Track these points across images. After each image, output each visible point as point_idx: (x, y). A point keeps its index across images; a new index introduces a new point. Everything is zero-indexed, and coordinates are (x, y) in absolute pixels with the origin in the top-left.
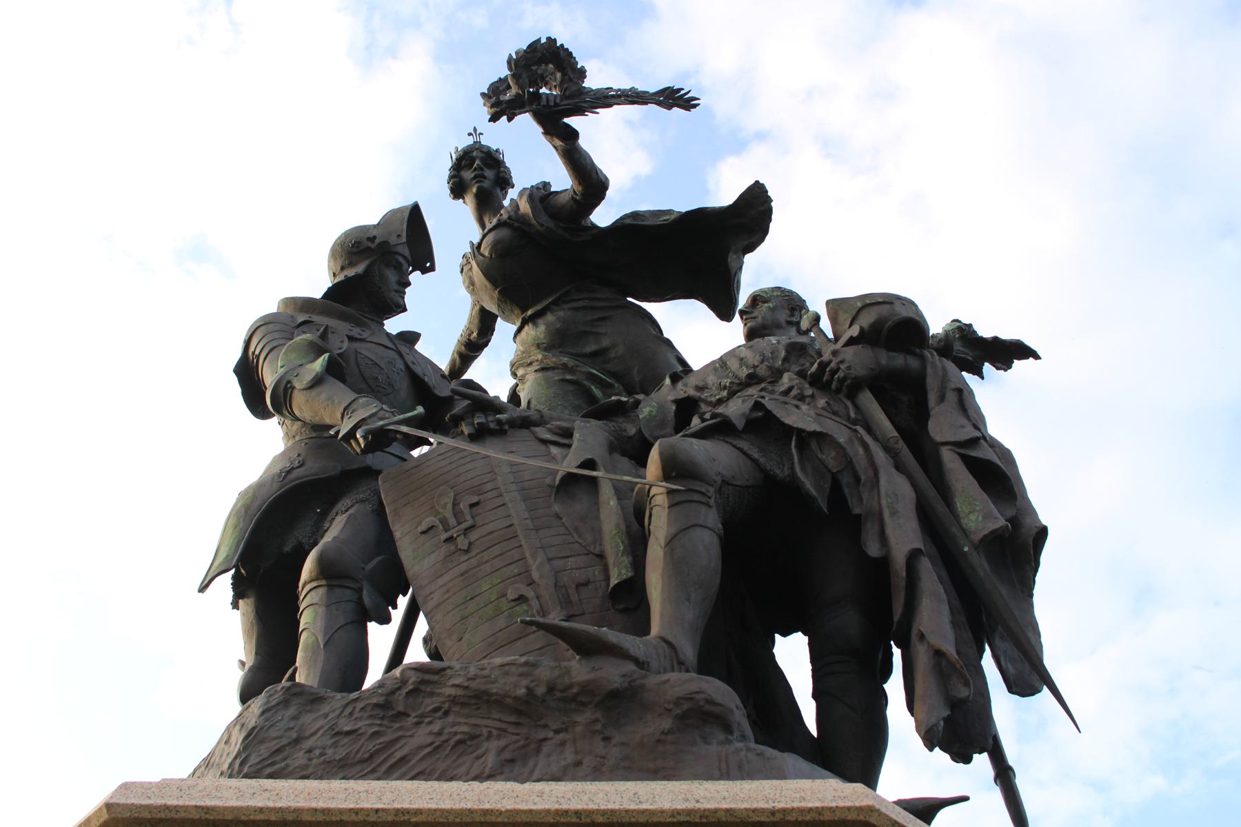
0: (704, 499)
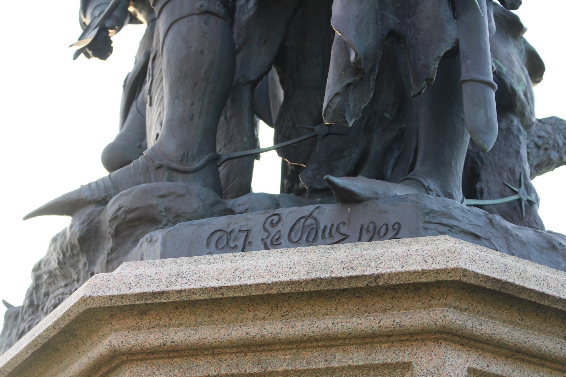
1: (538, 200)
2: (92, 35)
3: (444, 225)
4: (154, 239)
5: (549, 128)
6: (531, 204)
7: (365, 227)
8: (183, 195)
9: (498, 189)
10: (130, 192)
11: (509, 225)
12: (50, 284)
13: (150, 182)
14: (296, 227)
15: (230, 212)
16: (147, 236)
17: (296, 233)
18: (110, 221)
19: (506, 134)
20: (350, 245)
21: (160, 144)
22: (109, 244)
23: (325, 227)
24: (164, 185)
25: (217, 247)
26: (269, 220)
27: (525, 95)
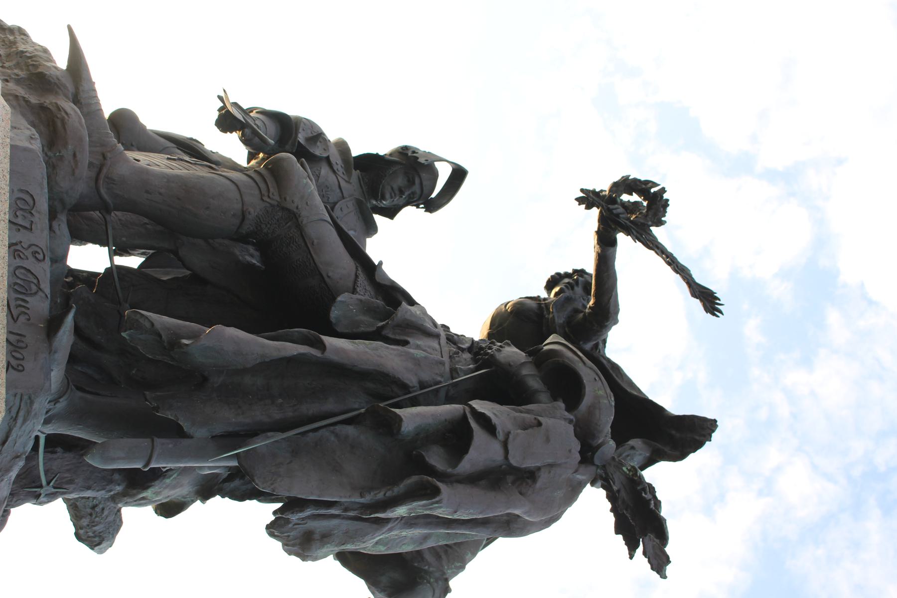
0: (264, 192)
1: (41, 504)
2: (239, 116)
3: (18, 413)
4: (33, 142)
5: (111, 518)
6: (36, 498)
7: (23, 339)
8: (73, 174)
9: (54, 468)
10: (82, 126)
11: (13, 474)
12: (4, 41)
13: (90, 146)
14: (29, 275)
15: (53, 215)
16: (37, 136)
17: (24, 274)
18: (56, 103)
19: (106, 478)
20: (5, 322)
21: (127, 160)
22: (34, 100)
23: (26, 302)
24: (85, 158)
25: (19, 199)
26: (39, 250)
27: (143, 498)
